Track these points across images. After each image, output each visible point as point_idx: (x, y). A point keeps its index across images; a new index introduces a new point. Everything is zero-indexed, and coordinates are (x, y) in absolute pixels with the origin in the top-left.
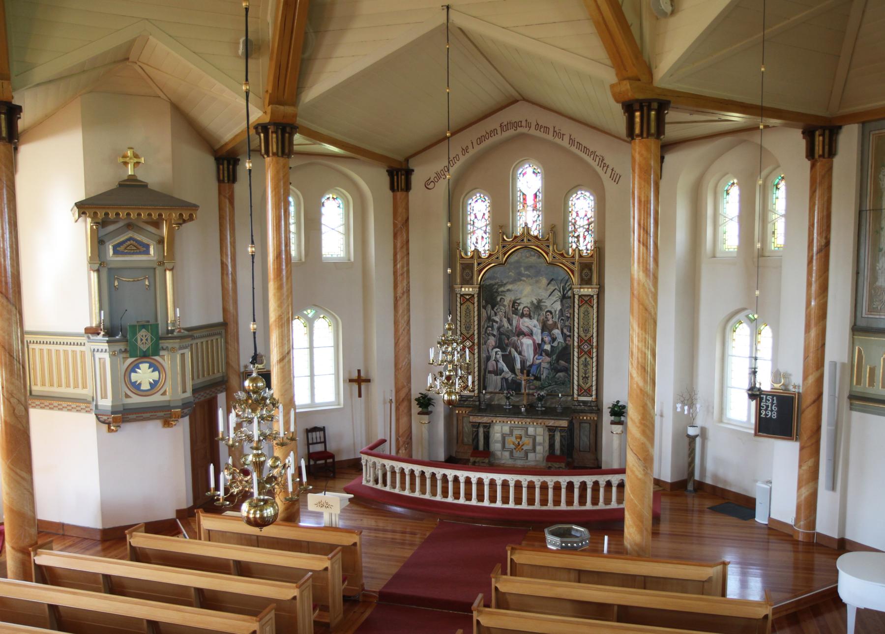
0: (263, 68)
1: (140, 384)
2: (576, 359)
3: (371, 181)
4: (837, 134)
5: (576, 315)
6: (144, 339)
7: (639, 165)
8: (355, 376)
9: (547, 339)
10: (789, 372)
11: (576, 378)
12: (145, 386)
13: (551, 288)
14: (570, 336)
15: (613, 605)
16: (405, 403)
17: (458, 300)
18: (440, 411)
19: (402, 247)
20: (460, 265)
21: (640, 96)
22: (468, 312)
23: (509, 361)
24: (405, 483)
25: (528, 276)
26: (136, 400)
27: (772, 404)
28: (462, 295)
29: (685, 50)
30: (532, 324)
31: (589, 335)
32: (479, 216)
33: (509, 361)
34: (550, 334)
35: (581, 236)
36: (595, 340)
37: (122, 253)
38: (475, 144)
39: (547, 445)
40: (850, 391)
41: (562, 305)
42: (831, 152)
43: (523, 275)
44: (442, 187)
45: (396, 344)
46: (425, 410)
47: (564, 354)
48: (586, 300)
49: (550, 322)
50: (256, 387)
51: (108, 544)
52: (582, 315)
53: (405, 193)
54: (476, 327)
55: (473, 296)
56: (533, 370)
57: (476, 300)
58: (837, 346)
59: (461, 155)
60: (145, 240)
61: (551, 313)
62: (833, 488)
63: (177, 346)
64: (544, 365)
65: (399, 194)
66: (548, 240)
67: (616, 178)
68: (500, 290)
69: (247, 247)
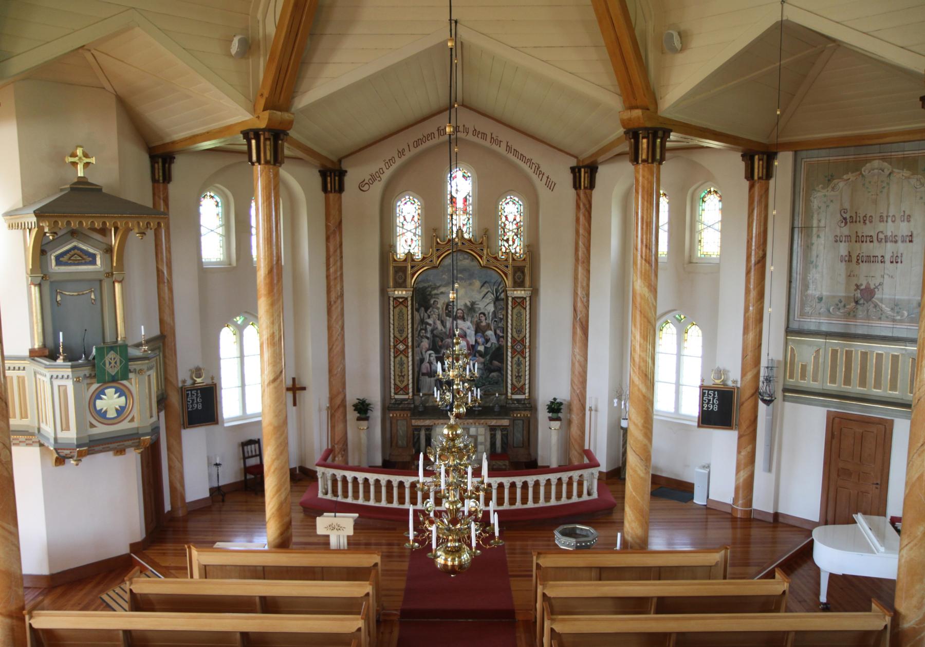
0: (261, 68)
1: (106, 412)
2: (509, 359)
5: (510, 317)
7: (643, 187)
9: (481, 340)
10: (727, 368)
11: (509, 377)
12: (112, 414)
13: (485, 290)
14: (503, 337)
15: (652, 598)
16: (341, 409)
17: (391, 303)
18: (376, 414)
19: (335, 251)
20: (394, 270)
21: (648, 125)
24: (369, 492)
26: (101, 429)
27: (714, 398)
28: (395, 299)
30: (466, 326)
31: (522, 336)
32: (409, 218)
34: (484, 336)
35: (511, 239)
36: (528, 340)
37: (66, 264)
38: (411, 147)
39: (488, 444)
40: (784, 385)
41: (495, 307)
44: (377, 188)
45: (330, 350)
46: (363, 416)
48: (519, 302)
49: (484, 324)
50: (456, 434)
51: (59, 591)
52: (515, 317)
53: (337, 195)
54: (410, 331)
55: (406, 299)
57: (410, 303)
58: (773, 347)
60: (91, 250)
61: (484, 314)
62: (770, 470)
63: (145, 367)
65: (331, 196)
66: (481, 243)
67: (551, 185)
68: (435, 292)
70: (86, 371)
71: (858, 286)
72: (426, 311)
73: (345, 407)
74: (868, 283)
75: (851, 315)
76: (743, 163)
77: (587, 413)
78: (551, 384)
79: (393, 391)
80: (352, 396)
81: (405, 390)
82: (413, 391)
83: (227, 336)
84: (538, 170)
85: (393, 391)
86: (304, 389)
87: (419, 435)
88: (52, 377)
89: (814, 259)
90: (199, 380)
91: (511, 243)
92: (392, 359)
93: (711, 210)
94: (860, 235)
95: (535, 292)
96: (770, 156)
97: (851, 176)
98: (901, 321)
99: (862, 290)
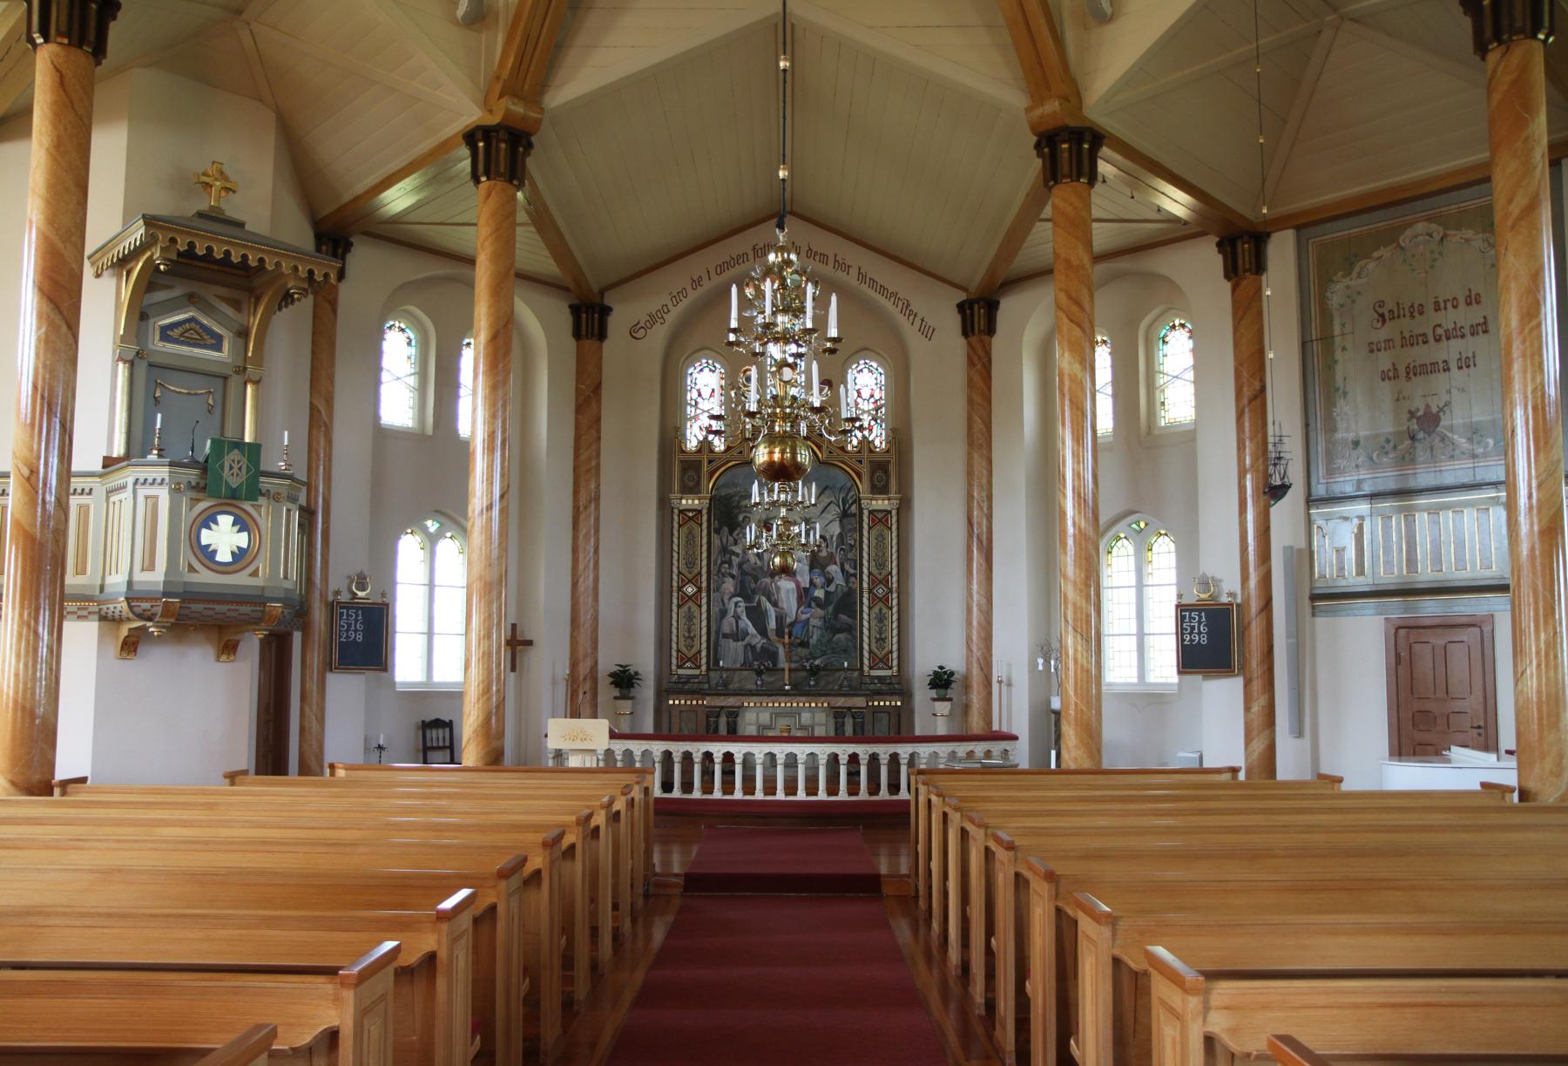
2: (866, 609)
3: (543, 324)
4: (1265, 242)
6: (236, 466)
9: (819, 581)
10: (1218, 577)
12: (224, 556)
13: (825, 500)
20: (679, 467)
22: (690, 538)
23: (757, 616)
27: (1200, 623)
29: (1148, 45)
32: (706, 393)
33: (757, 616)
34: (824, 573)
41: (842, 526)
42: (1259, 267)
44: (659, 336)
47: (846, 604)
48: (880, 518)
49: (824, 554)
52: (873, 541)
54: (704, 563)
55: (700, 512)
56: (797, 630)
57: (705, 518)
59: (689, 289)
60: (217, 329)
63: (284, 492)
64: (815, 622)
67: (927, 332)
70: (192, 475)
71: (1412, 414)
72: (731, 533)
73: (595, 681)
74: (1428, 406)
75: (1406, 460)
76: (1220, 258)
77: (995, 686)
78: (936, 642)
79: (674, 661)
80: (608, 662)
82: (708, 663)
83: (409, 548)
84: (907, 309)
85: (674, 661)
86: (530, 643)
87: (717, 724)
88: (136, 483)
89: (1339, 383)
90: (360, 594)
92: (675, 608)
93: (1177, 352)
95: (905, 505)
96: (1258, 239)
97: (1385, 252)
99: (1418, 418)
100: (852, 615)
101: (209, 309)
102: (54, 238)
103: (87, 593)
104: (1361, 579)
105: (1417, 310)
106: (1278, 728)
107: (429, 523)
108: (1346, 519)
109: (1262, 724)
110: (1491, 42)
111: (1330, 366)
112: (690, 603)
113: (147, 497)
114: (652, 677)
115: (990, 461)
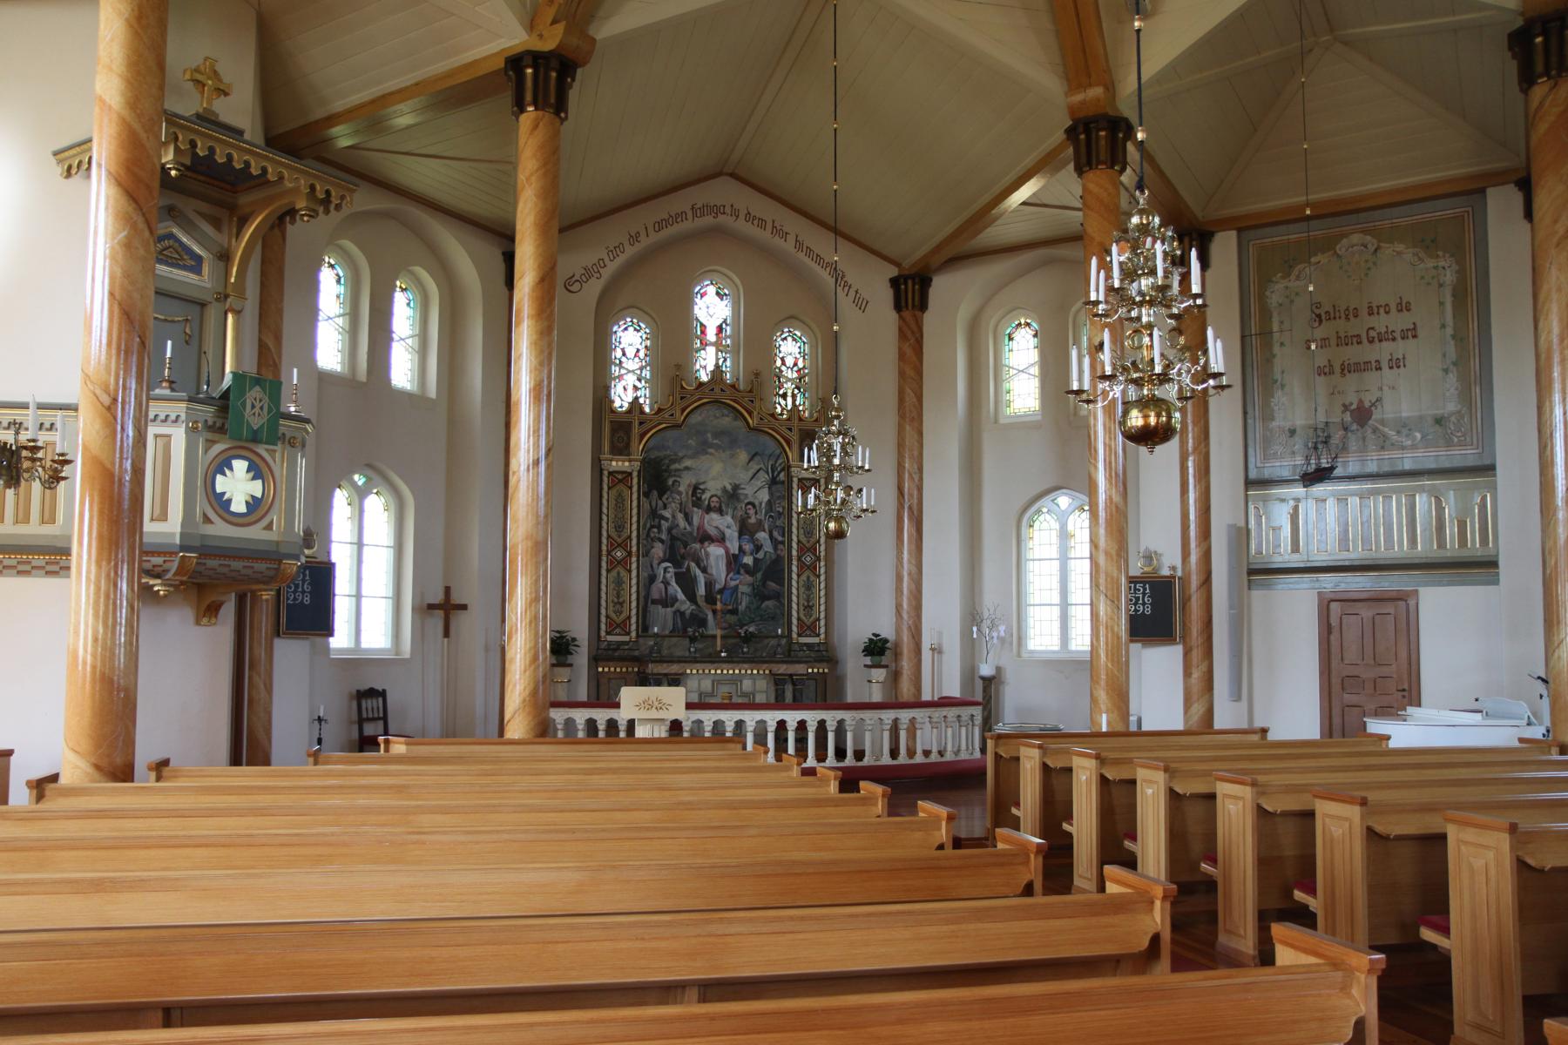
6: (258, 405)
8: (438, 597)
9: (748, 547)
12: (238, 506)
13: (755, 466)
14: (782, 543)
18: (581, 658)
23: (686, 582)
25: (717, 447)
28: (610, 473)
30: (724, 523)
32: (630, 352)
33: (686, 582)
34: (753, 540)
41: (771, 494)
43: (711, 446)
44: (595, 287)
47: (773, 571)
49: (753, 520)
55: (630, 474)
60: (197, 249)
64: (744, 589)
67: (861, 304)
68: (676, 466)
69: (1133, 20)
71: (1346, 407)
74: (1361, 401)
78: (864, 611)
81: (623, 627)
85: (603, 627)
86: (464, 607)
89: (1278, 376)
91: (789, 400)
94: (1342, 335)
98: (1414, 447)
100: (780, 582)
101: (189, 227)
102: (137, 127)
103: (59, 545)
104: (1296, 557)
105: (1352, 314)
106: (1216, 692)
107: (356, 477)
108: (1283, 500)
109: (1200, 688)
110: (1540, 76)
111: (1269, 360)
112: (619, 568)
113: (156, 436)
114: (586, 643)
115: (921, 434)
